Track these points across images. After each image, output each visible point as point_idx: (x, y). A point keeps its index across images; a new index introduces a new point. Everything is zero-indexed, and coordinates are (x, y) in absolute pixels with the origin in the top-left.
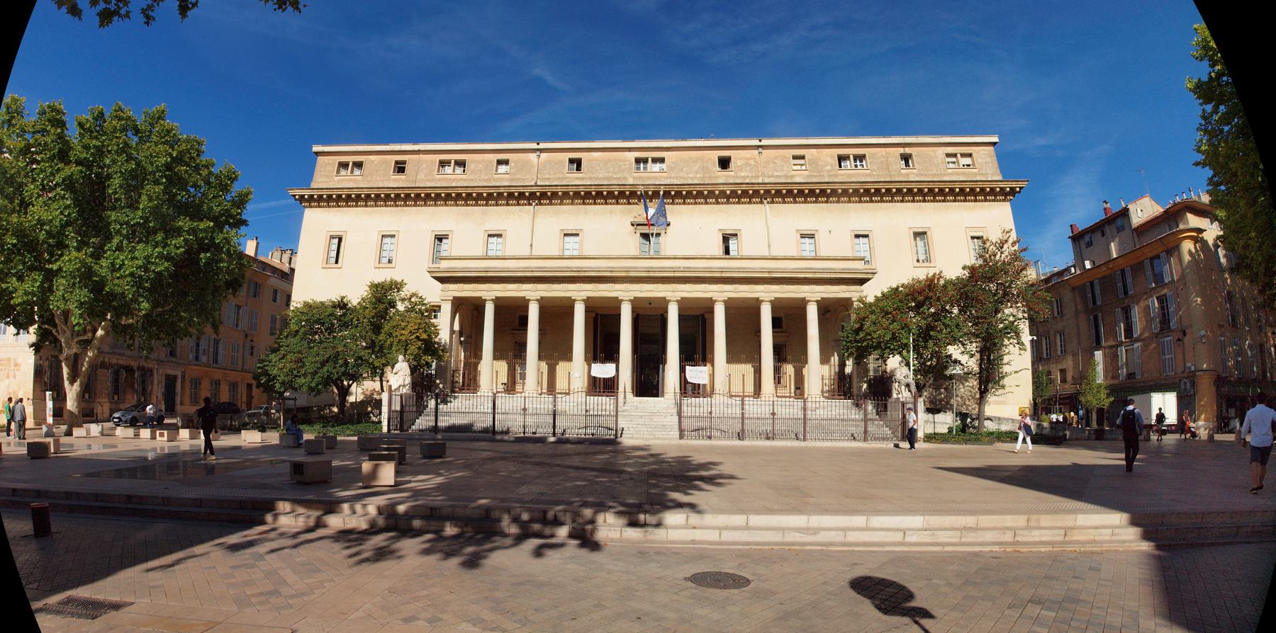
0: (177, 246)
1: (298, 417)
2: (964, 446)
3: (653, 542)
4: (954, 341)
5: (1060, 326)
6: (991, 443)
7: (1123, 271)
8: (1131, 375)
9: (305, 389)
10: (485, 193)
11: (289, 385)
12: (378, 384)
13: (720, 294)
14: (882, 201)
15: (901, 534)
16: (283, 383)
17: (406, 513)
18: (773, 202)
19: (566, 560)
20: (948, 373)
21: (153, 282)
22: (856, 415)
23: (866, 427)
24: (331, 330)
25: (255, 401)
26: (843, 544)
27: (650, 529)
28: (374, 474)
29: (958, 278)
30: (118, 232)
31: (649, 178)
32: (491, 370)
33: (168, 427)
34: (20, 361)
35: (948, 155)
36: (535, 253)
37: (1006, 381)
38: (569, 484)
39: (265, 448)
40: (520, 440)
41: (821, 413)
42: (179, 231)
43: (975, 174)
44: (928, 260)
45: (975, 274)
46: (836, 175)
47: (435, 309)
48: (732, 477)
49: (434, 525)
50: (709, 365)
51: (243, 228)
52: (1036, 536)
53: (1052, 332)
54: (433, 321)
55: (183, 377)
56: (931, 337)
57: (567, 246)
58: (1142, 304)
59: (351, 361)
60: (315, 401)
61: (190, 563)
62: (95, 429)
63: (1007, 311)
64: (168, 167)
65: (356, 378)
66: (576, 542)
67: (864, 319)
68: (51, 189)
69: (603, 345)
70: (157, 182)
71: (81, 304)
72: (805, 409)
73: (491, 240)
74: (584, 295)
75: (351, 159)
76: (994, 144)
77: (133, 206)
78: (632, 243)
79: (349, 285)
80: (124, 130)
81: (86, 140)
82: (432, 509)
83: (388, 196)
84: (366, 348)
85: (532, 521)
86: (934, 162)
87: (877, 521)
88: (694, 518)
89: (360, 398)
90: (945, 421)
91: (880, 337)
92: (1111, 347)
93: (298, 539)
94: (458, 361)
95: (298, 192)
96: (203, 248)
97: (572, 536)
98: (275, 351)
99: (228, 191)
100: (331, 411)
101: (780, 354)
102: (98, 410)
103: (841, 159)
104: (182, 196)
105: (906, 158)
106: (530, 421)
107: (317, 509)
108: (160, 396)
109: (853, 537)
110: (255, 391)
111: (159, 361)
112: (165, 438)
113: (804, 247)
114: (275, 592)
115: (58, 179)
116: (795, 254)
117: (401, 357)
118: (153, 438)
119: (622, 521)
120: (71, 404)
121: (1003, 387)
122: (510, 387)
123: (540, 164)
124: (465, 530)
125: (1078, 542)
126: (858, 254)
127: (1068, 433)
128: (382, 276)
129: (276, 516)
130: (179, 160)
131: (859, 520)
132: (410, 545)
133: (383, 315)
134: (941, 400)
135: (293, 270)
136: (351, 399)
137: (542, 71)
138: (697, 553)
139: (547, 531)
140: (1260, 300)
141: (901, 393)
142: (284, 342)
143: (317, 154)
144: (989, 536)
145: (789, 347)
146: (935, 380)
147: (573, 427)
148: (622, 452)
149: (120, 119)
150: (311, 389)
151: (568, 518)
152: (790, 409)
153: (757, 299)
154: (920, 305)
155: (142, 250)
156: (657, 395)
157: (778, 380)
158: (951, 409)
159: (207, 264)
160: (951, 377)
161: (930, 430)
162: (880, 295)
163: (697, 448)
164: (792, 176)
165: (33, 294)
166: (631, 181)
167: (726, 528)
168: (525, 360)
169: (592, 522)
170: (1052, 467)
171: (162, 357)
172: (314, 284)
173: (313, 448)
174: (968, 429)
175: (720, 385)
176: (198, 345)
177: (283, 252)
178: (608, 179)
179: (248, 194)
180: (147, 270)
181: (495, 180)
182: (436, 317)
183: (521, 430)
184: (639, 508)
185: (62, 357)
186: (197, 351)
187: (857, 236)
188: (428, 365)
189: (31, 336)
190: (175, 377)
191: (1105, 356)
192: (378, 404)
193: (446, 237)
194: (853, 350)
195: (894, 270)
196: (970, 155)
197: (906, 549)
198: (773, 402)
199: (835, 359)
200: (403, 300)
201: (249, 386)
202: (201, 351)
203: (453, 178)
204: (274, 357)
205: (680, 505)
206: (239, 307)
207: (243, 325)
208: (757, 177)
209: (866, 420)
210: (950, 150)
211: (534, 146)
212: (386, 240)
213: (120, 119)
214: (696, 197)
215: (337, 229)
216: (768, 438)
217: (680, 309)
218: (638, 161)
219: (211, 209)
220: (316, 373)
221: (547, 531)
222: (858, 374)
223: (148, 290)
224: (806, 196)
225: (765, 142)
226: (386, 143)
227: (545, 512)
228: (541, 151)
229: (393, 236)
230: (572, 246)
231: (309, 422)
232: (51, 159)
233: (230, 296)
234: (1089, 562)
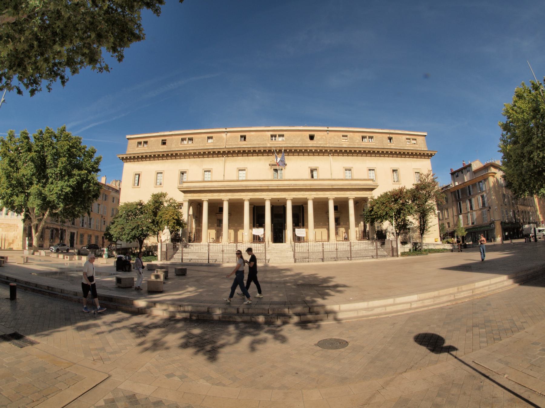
0: (73, 182)
7: (469, 187)
9: (125, 240)
11: (118, 239)
13: (310, 196)
15: (410, 304)
16: (116, 238)
18: (333, 155)
20: (408, 227)
21: (65, 195)
23: (377, 252)
24: (135, 215)
26: (386, 314)
29: (411, 189)
30: (51, 177)
31: (277, 144)
32: (208, 233)
34: (18, 225)
35: (407, 139)
36: (226, 179)
43: (417, 147)
44: (398, 181)
45: (418, 188)
46: (361, 145)
47: (180, 205)
48: (344, 286)
51: (99, 172)
55: (77, 233)
57: (240, 175)
58: (476, 198)
59: (144, 228)
60: (129, 245)
62: (43, 252)
64: (69, 150)
68: (26, 162)
69: (258, 220)
70: (64, 157)
71: (38, 205)
73: (206, 173)
75: (368, 135)
77: (56, 166)
78: (269, 174)
80: (50, 137)
81: (37, 143)
83: (159, 155)
84: (151, 223)
90: (408, 247)
94: (191, 228)
99: (92, 157)
101: (337, 220)
102: (45, 245)
103: (363, 138)
104: (74, 161)
105: (390, 139)
109: (389, 309)
110: (105, 241)
111: (68, 227)
112: (68, 259)
114: (103, 349)
115: (28, 158)
117: (166, 227)
118: (64, 258)
120: (35, 243)
123: (227, 138)
124: (204, 329)
126: (370, 178)
128: (157, 191)
130: (72, 147)
131: (390, 301)
133: (157, 208)
135: (120, 189)
140: (513, 197)
141: (390, 237)
143: (128, 139)
145: (341, 219)
149: (49, 133)
150: (127, 241)
152: (344, 246)
153: (327, 198)
155: (60, 183)
156: (282, 242)
157: (337, 233)
164: (342, 144)
165: (22, 202)
166: (269, 145)
168: (222, 227)
171: (70, 225)
174: (417, 249)
175: (311, 237)
176: (83, 220)
177: (116, 181)
178: (259, 144)
179: (100, 158)
180: (62, 191)
181: (206, 146)
182: (181, 208)
185: (32, 225)
186: (83, 223)
187: (370, 170)
188: (178, 230)
189: (22, 216)
190: (74, 233)
191: (463, 217)
193: (185, 172)
194: (369, 219)
195: (385, 186)
196: (415, 140)
197: (413, 311)
199: (362, 223)
200: (166, 201)
201: (103, 238)
203: (187, 146)
206: (99, 205)
207: (101, 212)
208: (326, 144)
209: (377, 249)
210: (408, 137)
211: (224, 130)
213: (49, 133)
215: (138, 171)
217: (293, 203)
218: (272, 136)
223: (63, 199)
225: (330, 129)
226: (158, 132)
228: (227, 132)
229: (161, 173)
232: (26, 151)
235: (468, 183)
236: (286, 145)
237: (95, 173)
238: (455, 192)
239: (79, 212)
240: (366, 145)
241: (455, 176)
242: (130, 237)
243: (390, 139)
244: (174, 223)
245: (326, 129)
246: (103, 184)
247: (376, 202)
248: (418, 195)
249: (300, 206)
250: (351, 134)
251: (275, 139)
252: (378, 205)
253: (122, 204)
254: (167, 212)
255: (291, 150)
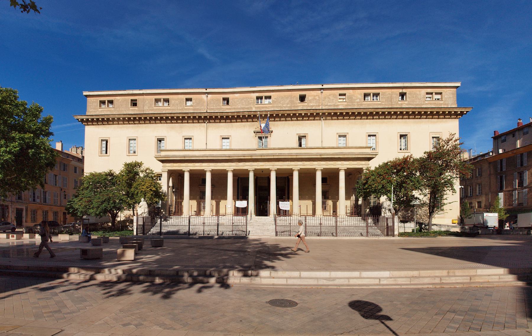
0: (15, 146)
1: (89, 228)
2: (420, 238)
3: (254, 284)
4: (416, 188)
5: (479, 181)
6: (435, 236)
8: (520, 204)
9: (93, 215)
10: (181, 116)
12: (132, 212)
14: (385, 118)
15: (378, 280)
16: (82, 212)
17: (137, 272)
18: (326, 119)
19: (213, 294)
20: (412, 203)
22: (363, 224)
23: (367, 230)
25: (68, 221)
27: (253, 278)
28: (123, 254)
29: (421, 158)
31: (263, 107)
32: (189, 205)
33: (18, 233)
35: (427, 93)
36: (208, 148)
37: (445, 207)
38: (220, 258)
39: (71, 243)
40: (201, 238)
41: (345, 223)
42: (13, 139)
43: (441, 104)
44: (406, 149)
46: (361, 105)
47: (159, 176)
49: (150, 279)
50: (290, 201)
51: (51, 136)
52: (453, 280)
53: (474, 184)
54: (159, 181)
56: (403, 187)
57: (224, 144)
61: (15, 297)
63: (447, 174)
65: (120, 209)
66: (218, 285)
67: (368, 179)
72: (336, 222)
73: (186, 141)
74: (232, 168)
76: (457, 87)
79: (115, 163)
82: (150, 271)
85: (199, 275)
86: (418, 97)
87: (365, 274)
88: (274, 274)
89: (123, 219)
90: (410, 227)
91: (376, 187)
92: (509, 191)
93: (79, 286)
94: (172, 201)
95: (80, 117)
96: (29, 147)
97: (217, 282)
98: (76, 197)
99: (38, 118)
100: (108, 225)
101: (325, 196)
103: (366, 95)
105: (403, 95)
106: (206, 228)
107: (92, 271)
108: (13, 218)
109: (352, 282)
110: (68, 216)
112: (15, 238)
113: (340, 142)
114: (59, 311)
116: (335, 146)
117: (142, 199)
119: (240, 274)
121: (443, 210)
122: (198, 213)
123: (207, 101)
124: (166, 281)
125: (479, 282)
126: (369, 145)
127: (480, 231)
128: (131, 160)
129: (69, 275)
131: (356, 274)
132: (137, 288)
134: (408, 217)
135: (83, 157)
136: (118, 219)
137: (202, 50)
138: (275, 290)
139: (205, 280)
141: (386, 214)
142: (81, 192)
144: (426, 281)
145: (331, 192)
146: (405, 207)
147: (226, 231)
148: (248, 242)
151: (216, 275)
152: (329, 221)
154: (398, 171)
156: (267, 216)
157: (324, 207)
158: (413, 221)
159: (33, 155)
160: (414, 206)
161: (402, 231)
162: (378, 166)
163: (284, 240)
164: (338, 105)
166: (254, 110)
167: (290, 278)
169: (227, 275)
170: (469, 247)
172: (94, 164)
173: (96, 243)
174: (423, 230)
175: (296, 210)
176: (34, 194)
178: (243, 108)
179: (50, 119)
181: (185, 109)
182: (160, 180)
183: (202, 233)
184: (249, 268)
186: (34, 197)
187: (369, 136)
188: (157, 203)
190: (22, 210)
191: (505, 195)
192: (132, 221)
193: (163, 139)
195: (387, 153)
196: (441, 93)
197: (381, 287)
198: (321, 218)
199: (353, 198)
200: (142, 171)
201: (64, 213)
202: (36, 197)
203: (163, 108)
204: (76, 200)
205: (267, 267)
206: (56, 176)
207: (59, 184)
208: (319, 106)
209: (367, 226)
210: (429, 90)
211: (204, 91)
212: (131, 142)
214: (286, 117)
215: (105, 136)
216: (318, 236)
218: (258, 98)
219: (30, 127)
220: (99, 207)
221: (205, 280)
222: (365, 204)
224: (344, 116)
225: (209, 90)
226: (125, 90)
227: (205, 271)
228: (208, 93)
229: (135, 140)
230: (226, 144)
231: (96, 230)
233: (49, 171)
234: (487, 291)
235: (521, 149)
236: (272, 109)
237: (46, 138)
238: (495, 162)
239: (28, 184)
240: (368, 105)
241: (500, 140)
242: (99, 210)
243: (403, 95)
244: (152, 195)
245: (204, 91)
246: (58, 151)
247: (372, 173)
248: (432, 168)
249: (285, 178)
250: (351, 91)
251: (261, 102)
252: (373, 177)
253: (88, 175)
254: (143, 183)
255: (278, 114)
